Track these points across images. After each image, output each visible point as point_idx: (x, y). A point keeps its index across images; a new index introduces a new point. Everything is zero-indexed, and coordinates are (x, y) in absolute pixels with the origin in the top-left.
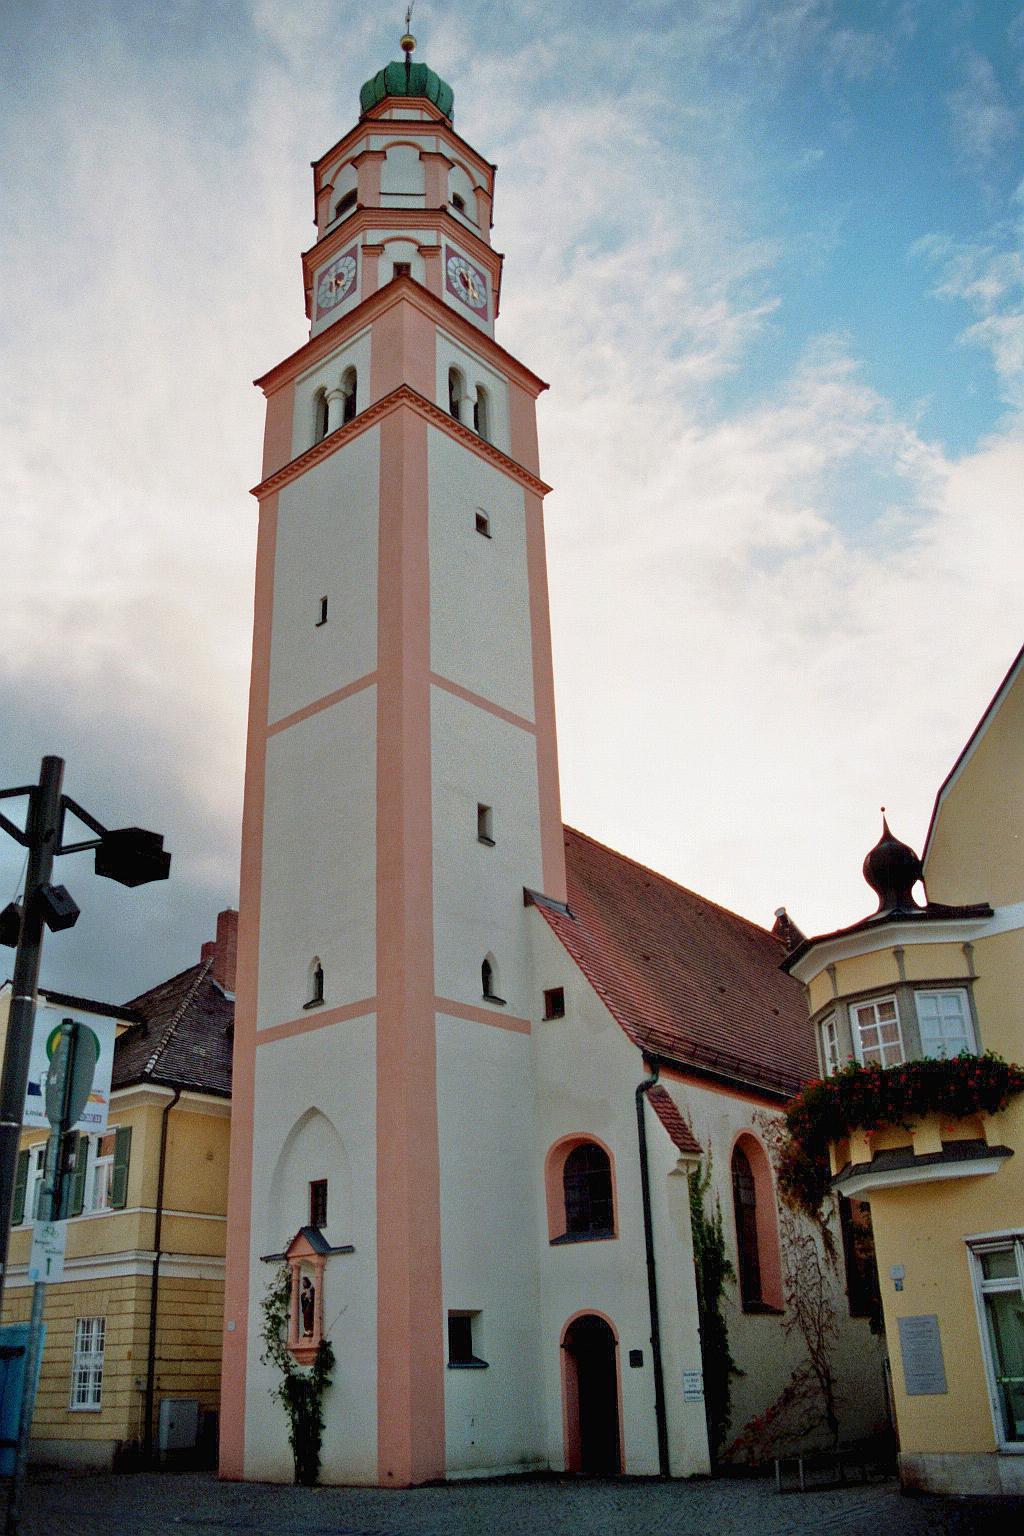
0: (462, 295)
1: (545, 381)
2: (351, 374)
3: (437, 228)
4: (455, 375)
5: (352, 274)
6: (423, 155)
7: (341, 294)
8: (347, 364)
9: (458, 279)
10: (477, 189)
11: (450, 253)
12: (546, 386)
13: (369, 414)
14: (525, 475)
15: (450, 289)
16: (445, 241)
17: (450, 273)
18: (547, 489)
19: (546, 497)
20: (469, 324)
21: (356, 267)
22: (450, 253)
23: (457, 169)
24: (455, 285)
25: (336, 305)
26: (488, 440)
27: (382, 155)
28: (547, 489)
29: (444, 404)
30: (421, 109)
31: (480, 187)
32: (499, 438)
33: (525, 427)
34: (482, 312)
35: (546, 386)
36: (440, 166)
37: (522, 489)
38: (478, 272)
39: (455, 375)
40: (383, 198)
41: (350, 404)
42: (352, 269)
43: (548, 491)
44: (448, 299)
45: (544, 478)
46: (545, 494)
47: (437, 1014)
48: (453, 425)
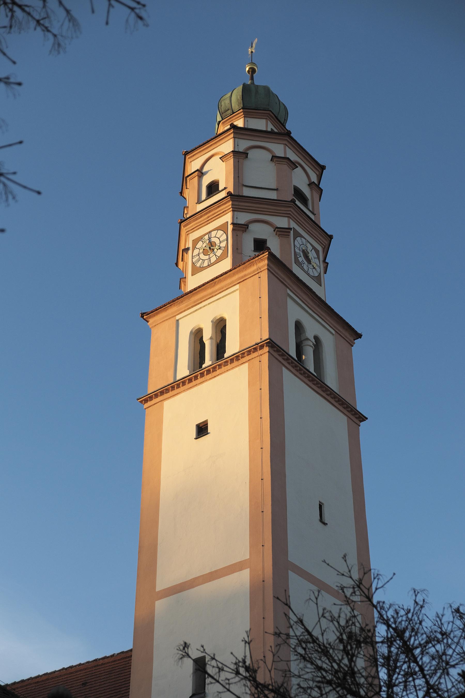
0: (305, 267)
1: (359, 332)
2: (220, 326)
3: (289, 216)
4: (299, 326)
5: (223, 244)
6: (274, 158)
7: (213, 259)
8: (218, 314)
9: (301, 254)
10: (311, 184)
11: (297, 235)
12: (359, 336)
13: (237, 357)
14: (352, 411)
15: (297, 262)
16: (293, 225)
17: (297, 251)
18: (363, 418)
19: (362, 424)
20: (317, 296)
21: (227, 239)
22: (297, 235)
23: (299, 169)
24: (300, 259)
25: (209, 266)
26: (322, 380)
27: (244, 156)
28: (363, 418)
29: (293, 352)
30: (266, 119)
31: (313, 182)
32: (331, 379)
33: (346, 365)
34: (318, 280)
35: (359, 336)
36: (285, 167)
37: (346, 418)
38: (314, 248)
39: (299, 326)
40: (245, 188)
41: (220, 348)
42: (223, 241)
43: (363, 420)
44: (296, 270)
45: (360, 408)
46: (361, 421)
47: (158, 589)
48: (296, 366)
